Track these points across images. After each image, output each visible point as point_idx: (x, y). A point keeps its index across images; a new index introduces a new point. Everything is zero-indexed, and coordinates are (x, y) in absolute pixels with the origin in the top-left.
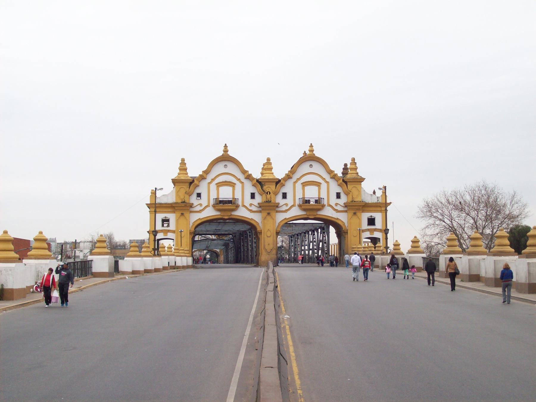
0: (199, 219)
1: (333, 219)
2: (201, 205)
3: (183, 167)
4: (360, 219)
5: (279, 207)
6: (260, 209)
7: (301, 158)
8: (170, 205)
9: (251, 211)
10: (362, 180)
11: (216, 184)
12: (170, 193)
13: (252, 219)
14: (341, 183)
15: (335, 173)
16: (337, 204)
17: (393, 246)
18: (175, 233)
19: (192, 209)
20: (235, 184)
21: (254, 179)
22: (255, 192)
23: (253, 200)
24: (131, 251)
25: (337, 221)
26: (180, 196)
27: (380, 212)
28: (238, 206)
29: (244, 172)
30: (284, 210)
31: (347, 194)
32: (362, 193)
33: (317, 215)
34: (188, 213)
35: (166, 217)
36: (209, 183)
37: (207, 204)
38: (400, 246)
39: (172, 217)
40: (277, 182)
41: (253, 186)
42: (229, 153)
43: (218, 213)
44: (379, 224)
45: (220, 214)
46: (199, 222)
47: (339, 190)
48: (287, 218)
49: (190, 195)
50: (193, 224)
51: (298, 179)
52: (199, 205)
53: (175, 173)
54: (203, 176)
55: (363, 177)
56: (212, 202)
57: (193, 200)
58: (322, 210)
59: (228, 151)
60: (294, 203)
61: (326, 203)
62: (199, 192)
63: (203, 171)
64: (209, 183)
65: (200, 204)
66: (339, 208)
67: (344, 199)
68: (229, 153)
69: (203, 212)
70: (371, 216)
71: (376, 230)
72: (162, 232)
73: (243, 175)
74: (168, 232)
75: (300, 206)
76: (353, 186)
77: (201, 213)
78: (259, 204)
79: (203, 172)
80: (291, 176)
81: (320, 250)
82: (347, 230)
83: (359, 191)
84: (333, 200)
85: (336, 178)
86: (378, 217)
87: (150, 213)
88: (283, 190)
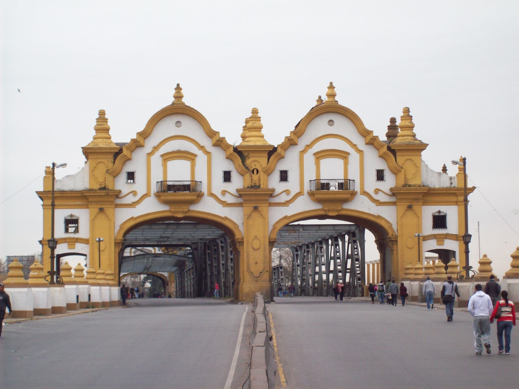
0: (132, 218)
4: (419, 217)
6: (240, 200)
7: (313, 108)
9: (378, 203)
10: (422, 146)
11: (162, 156)
14: (384, 153)
16: (377, 191)
17: (479, 265)
18: (88, 244)
19: (119, 201)
20: (196, 156)
21: (229, 146)
22: (230, 170)
23: (227, 184)
24: (9, 277)
25: (378, 221)
28: (200, 195)
29: (211, 134)
31: (395, 172)
32: (423, 168)
33: (342, 209)
35: (439, 212)
37: (298, 190)
38: (491, 265)
40: (270, 151)
43: (166, 208)
47: (381, 165)
49: (115, 175)
50: (274, 227)
55: (425, 141)
56: (154, 189)
59: (182, 97)
61: (357, 188)
62: (284, 168)
65: (286, 191)
66: (229, 199)
69: (138, 207)
70: (439, 212)
71: (448, 236)
75: (311, 194)
83: (418, 167)
85: (375, 143)
87: (44, 209)
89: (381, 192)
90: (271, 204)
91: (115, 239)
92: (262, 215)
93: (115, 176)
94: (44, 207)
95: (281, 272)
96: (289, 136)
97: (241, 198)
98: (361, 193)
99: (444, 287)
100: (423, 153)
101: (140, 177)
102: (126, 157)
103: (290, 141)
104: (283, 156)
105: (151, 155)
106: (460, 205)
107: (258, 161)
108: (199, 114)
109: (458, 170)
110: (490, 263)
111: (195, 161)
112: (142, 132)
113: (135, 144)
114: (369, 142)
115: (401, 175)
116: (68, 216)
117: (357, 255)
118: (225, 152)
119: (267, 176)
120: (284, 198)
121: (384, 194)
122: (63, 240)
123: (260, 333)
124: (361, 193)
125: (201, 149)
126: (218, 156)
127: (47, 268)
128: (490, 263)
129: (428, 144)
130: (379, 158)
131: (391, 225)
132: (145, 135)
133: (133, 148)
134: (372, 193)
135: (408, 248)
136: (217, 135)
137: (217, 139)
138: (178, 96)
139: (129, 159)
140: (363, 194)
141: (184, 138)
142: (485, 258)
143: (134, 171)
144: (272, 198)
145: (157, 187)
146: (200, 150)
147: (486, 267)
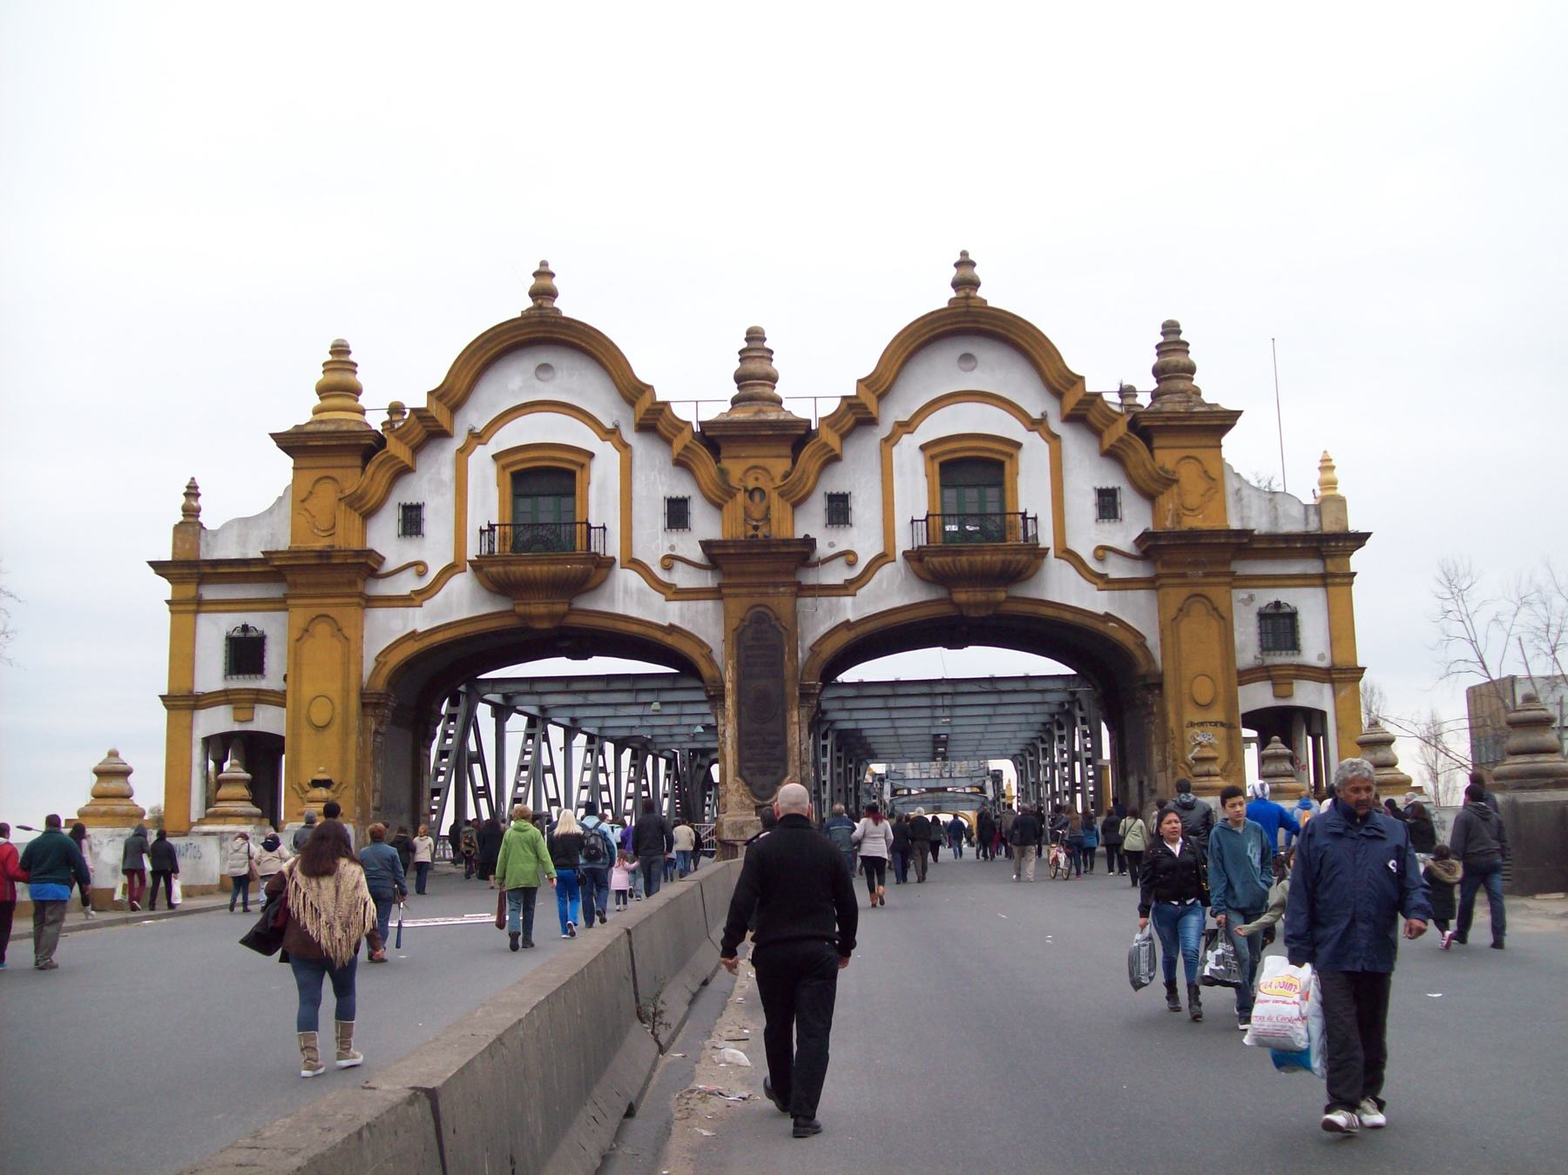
0: (413, 635)
1: (1089, 622)
2: (421, 568)
4: (1225, 622)
5: (815, 565)
8: (311, 557)
9: (674, 593)
10: (1224, 421)
12: (270, 511)
13: (1107, 614)
14: (1121, 440)
16: (669, 561)
17: (95, 778)
18: (283, 705)
19: (811, 578)
20: (1018, 445)
22: (686, 496)
23: (1107, 526)
26: (313, 517)
29: (632, 391)
31: (1149, 492)
34: (188, 612)
35: (245, 628)
37: (878, 549)
38: (131, 778)
39: (273, 626)
41: (678, 469)
42: (981, 293)
44: (1314, 646)
46: (844, 638)
47: (1111, 478)
48: (420, 630)
49: (369, 514)
50: (381, 659)
51: (906, 427)
52: (841, 560)
54: (863, 406)
55: (1228, 405)
57: (384, 536)
58: (1034, 580)
60: (885, 545)
61: (1046, 539)
62: (410, 500)
63: (860, 381)
64: (886, 440)
66: (683, 578)
67: (1135, 520)
68: (981, 293)
70: (245, 628)
71: (261, 697)
72: (228, 702)
73: (626, 406)
75: (914, 557)
76: (752, 462)
78: (706, 545)
81: (1079, 791)
82: (1161, 675)
83: (1215, 478)
84: (653, 541)
85: (1093, 416)
86: (1310, 607)
87: (171, 611)
89: (679, 562)
91: (363, 694)
92: (339, 630)
93: (368, 514)
94: (175, 608)
96: (854, 393)
98: (1058, 555)
99: (1431, 802)
100: (1227, 440)
101: (865, 509)
102: (396, 461)
103: (425, 424)
104: (838, 451)
106: (1335, 585)
107: (765, 469)
109: (181, 513)
110: (126, 773)
111: (1017, 459)
112: (873, 373)
113: (424, 427)
114: (1074, 412)
115: (1168, 502)
116: (235, 630)
117: (446, 735)
119: (789, 507)
120: (406, 584)
121: (1126, 559)
122: (253, 694)
123: (402, 942)
124: (1059, 554)
125: (607, 437)
127: (1445, 738)
128: (126, 773)
130: (1102, 458)
131: (707, 651)
132: (880, 384)
133: (847, 427)
134: (1086, 554)
135: (1197, 704)
136: (647, 394)
137: (1080, 396)
139: (835, 458)
140: (1064, 555)
141: (533, 409)
142: (114, 760)
143: (847, 492)
144: (381, 581)
145: (481, 546)
147: (114, 785)
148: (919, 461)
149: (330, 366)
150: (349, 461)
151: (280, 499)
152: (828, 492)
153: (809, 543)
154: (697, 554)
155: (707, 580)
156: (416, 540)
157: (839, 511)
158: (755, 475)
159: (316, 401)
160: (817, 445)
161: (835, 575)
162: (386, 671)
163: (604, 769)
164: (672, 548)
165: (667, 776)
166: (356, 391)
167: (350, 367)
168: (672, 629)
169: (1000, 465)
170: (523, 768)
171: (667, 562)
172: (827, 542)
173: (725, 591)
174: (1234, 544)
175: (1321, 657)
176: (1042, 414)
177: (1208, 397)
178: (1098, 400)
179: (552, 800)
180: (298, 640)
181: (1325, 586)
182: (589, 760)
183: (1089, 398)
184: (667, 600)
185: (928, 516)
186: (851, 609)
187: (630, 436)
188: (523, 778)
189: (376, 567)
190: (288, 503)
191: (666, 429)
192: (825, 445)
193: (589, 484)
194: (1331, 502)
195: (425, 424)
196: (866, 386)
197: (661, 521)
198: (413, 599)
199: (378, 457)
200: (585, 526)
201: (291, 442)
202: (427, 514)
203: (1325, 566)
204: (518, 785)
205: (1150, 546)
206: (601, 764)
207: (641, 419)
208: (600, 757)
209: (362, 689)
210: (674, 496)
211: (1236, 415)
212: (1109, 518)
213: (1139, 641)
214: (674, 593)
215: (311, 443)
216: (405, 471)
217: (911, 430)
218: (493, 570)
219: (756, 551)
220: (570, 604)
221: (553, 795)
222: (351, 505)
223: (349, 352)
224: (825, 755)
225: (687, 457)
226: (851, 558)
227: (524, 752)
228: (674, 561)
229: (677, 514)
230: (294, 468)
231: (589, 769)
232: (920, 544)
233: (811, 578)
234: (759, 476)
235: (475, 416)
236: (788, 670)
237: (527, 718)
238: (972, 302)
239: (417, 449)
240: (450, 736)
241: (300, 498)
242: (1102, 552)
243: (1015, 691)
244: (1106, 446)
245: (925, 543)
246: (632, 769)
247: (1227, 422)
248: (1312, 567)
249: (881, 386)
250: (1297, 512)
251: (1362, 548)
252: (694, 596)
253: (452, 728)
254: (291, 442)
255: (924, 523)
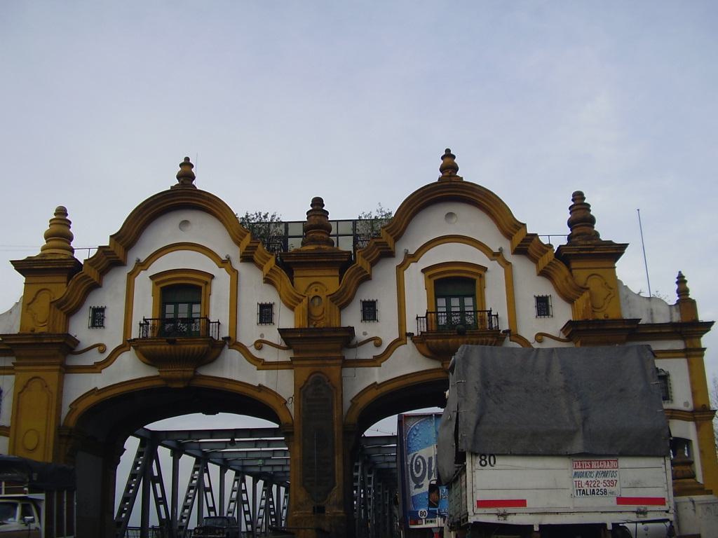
0: (94, 391)
2: (101, 348)
3: (60, 229)
6: (285, 356)
9: (263, 365)
10: (616, 251)
11: (152, 277)
12: (10, 312)
15: (529, 231)
16: (260, 344)
18: (7, 435)
19: (350, 355)
20: (485, 269)
22: (272, 302)
23: (543, 320)
27: (684, 355)
30: (91, 363)
32: (623, 293)
36: (401, 268)
43: (152, 372)
44: (681, 397)
45: (158, 373)
49: (72, 312)
53: (33, 246)
55: (618, 240)
57: (80, 328)
59: (457, 169)
63: (111, 236)
66: (269, 355)
67: (562, 313)
73: (508, 238)
74: (672, 418)
77: (100, 372)
78: (282, 331)
79: (113, 240)
80: (391, 245)
85: (532, 249)
86: (677, 370)
88: (96, 300)
90: (347, 363)
95: (386, 493)
97: (288, 351)
100: (619, 264)
101: (387, 310)
105: (402, 269)
108: (221, 203)
118: (535, 263)
120: (94, 358)
125: (223, 265)
126: (524, 270)
129: (12, 262)
138: (186, 173)
139: (368, 278)
144: (75, 356)
146: (220, 267)
148: (421, 278)
149: (53, 222)
150: (57, 279)
151: (17, 303)
152: (363, 300)
153: (351, 330)
154: (275, 337)
155: (285, 356)
156: (99, 330)
157: (370, 311)
158: (314, 289)
159: (44, 242)
160: (354, 269)
161: (368, 352)
162: (75, 415)
163: (245, 491)
164: (262, 335)
165: (286, 497)
166: (70, 238)
167: (67, 223)
168: (261, 388)
169: (473, 282)
170: (190, 488)
171: (258, 345)
172: (363, 330)
173: (295, 363)
174: (628, 329)
175: (686, 404)
176: (499, 249)
177: (604, 237)
178: (535, 239)
179: (211, 508)
180: (20, 393)
181: (687, 357)
182: (236, 485)
183: (529, 237)
184: (258, 369)
185: (427, 313)
186: (377, 375)
187: (238, 265)
188: (191, 494)
189: (73, 347)
190: (20, 306)
191: (260, 260)
192: (361, 268)
193: (210, 295)
194: (685, 301)
195: (108, 256)
196: (387, 231)
197: (256, 318)
198: (96, 368)
199: (77, 277)
200: (217, 324)
201: (23, 266)
202: (108, 314)
203: (686, 344)
204: (187, 498)
205: (573, 330)
206: (243, 488)
207: (243, 253)
208: (243, 484)
209: (60, 426)
210: (264, 303)
211: (624, 246)
212: (544, 315)
213: (262, 362)
214: (263, 365)
215: (35, 267)
216: (96, 286)
217: (146, 268)
218: (144, 347)
219: (314, 335)
220: (195, 372)
221: (211, 505)
222: (59, 307)
223: (67, 215)
224: (357, 471)
225: (272, 277)
226: (378, 342)
227: (192, 479)
228: (263, 344)
229: (266, 313)
230: (25, 284)
231: (235, 491)
232: (422, 330)
233: (350, 355)
234: (318, 288)
235: (141, 252)
236: (336, 415)
237: (139, 440)
238: (453, 179)
239: (104, 272)
240: (139, 465)
241: (28, 303)
242: (540, 337)
243: (43, 365)
244: (541, 267)
245: (426, 331)
246: (264, 492)
247: (619, 251)
248: (679, 345)
249: (397, 231)
250: (665, 310)
251: (709, 332)
252: (276, 366)
253: (141, 460)
254: (23, 266)
255: (425, 319)
